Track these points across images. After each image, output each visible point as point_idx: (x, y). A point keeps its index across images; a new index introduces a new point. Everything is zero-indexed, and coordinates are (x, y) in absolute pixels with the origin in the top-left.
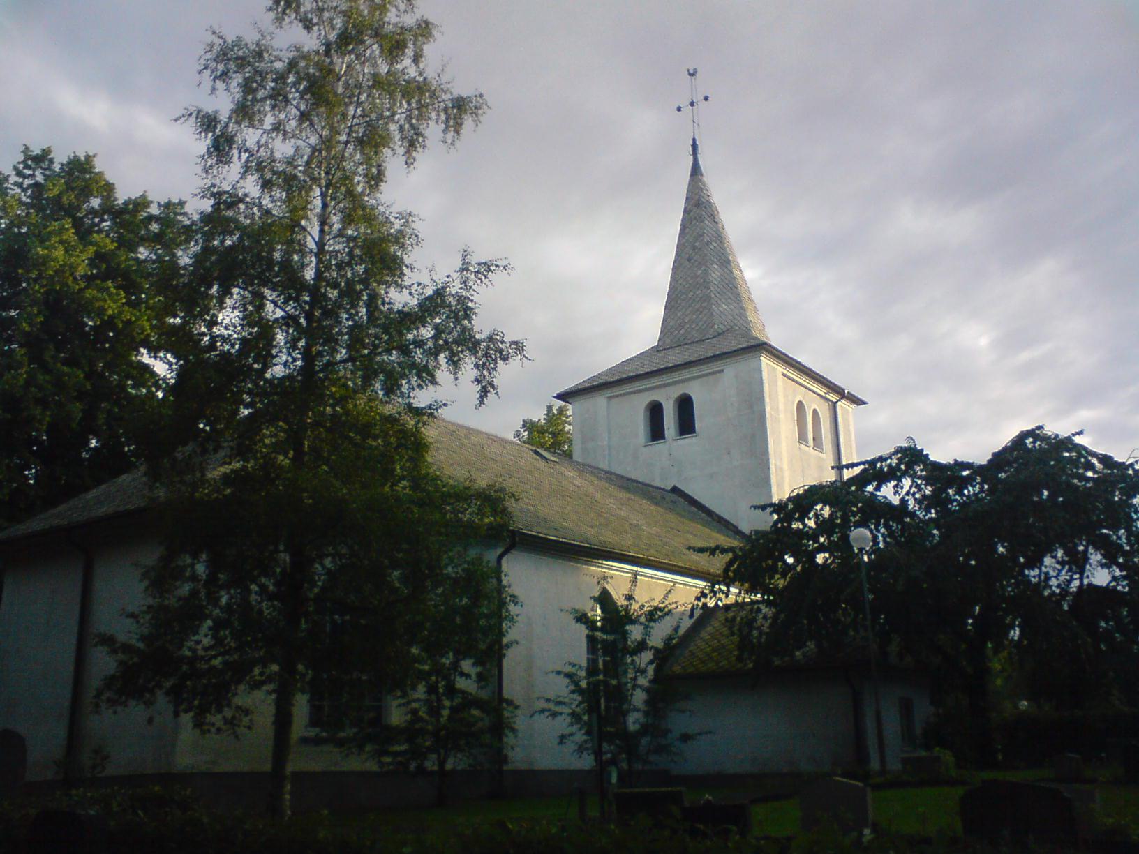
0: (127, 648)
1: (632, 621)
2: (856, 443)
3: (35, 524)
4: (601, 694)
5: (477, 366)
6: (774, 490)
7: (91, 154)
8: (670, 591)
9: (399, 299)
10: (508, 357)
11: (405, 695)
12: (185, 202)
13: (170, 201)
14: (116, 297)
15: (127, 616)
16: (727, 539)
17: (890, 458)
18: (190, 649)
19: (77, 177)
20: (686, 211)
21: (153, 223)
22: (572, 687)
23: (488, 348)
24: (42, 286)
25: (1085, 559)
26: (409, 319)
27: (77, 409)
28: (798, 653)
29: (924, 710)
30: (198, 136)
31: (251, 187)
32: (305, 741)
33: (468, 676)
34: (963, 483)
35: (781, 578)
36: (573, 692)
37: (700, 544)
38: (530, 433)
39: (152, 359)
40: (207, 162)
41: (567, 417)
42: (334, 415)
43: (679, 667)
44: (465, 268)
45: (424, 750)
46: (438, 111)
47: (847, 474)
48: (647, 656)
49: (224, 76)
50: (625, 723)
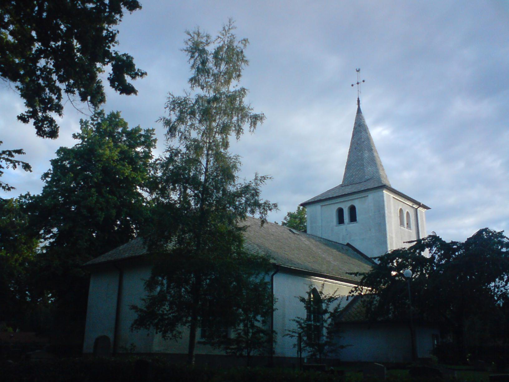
0: (141, 310)
3: (102, 259)
5: (260, 213)
6: (389, 246)
8: (336, 291)
9: (231, 189)
11: (235, 328)
12: (155, 129)
13: (149, 129)
16: (369, 266)
17: (427, 239)
20: (355, 128)
22: (299, 326)
26: (238, 195)
27: (114, 212)
32: (199, 343)
33: (259, 321)
39: (142, 190)
40: (167, 136)
44: (256, 179)
45: (242, 348)
49: (173, 109)
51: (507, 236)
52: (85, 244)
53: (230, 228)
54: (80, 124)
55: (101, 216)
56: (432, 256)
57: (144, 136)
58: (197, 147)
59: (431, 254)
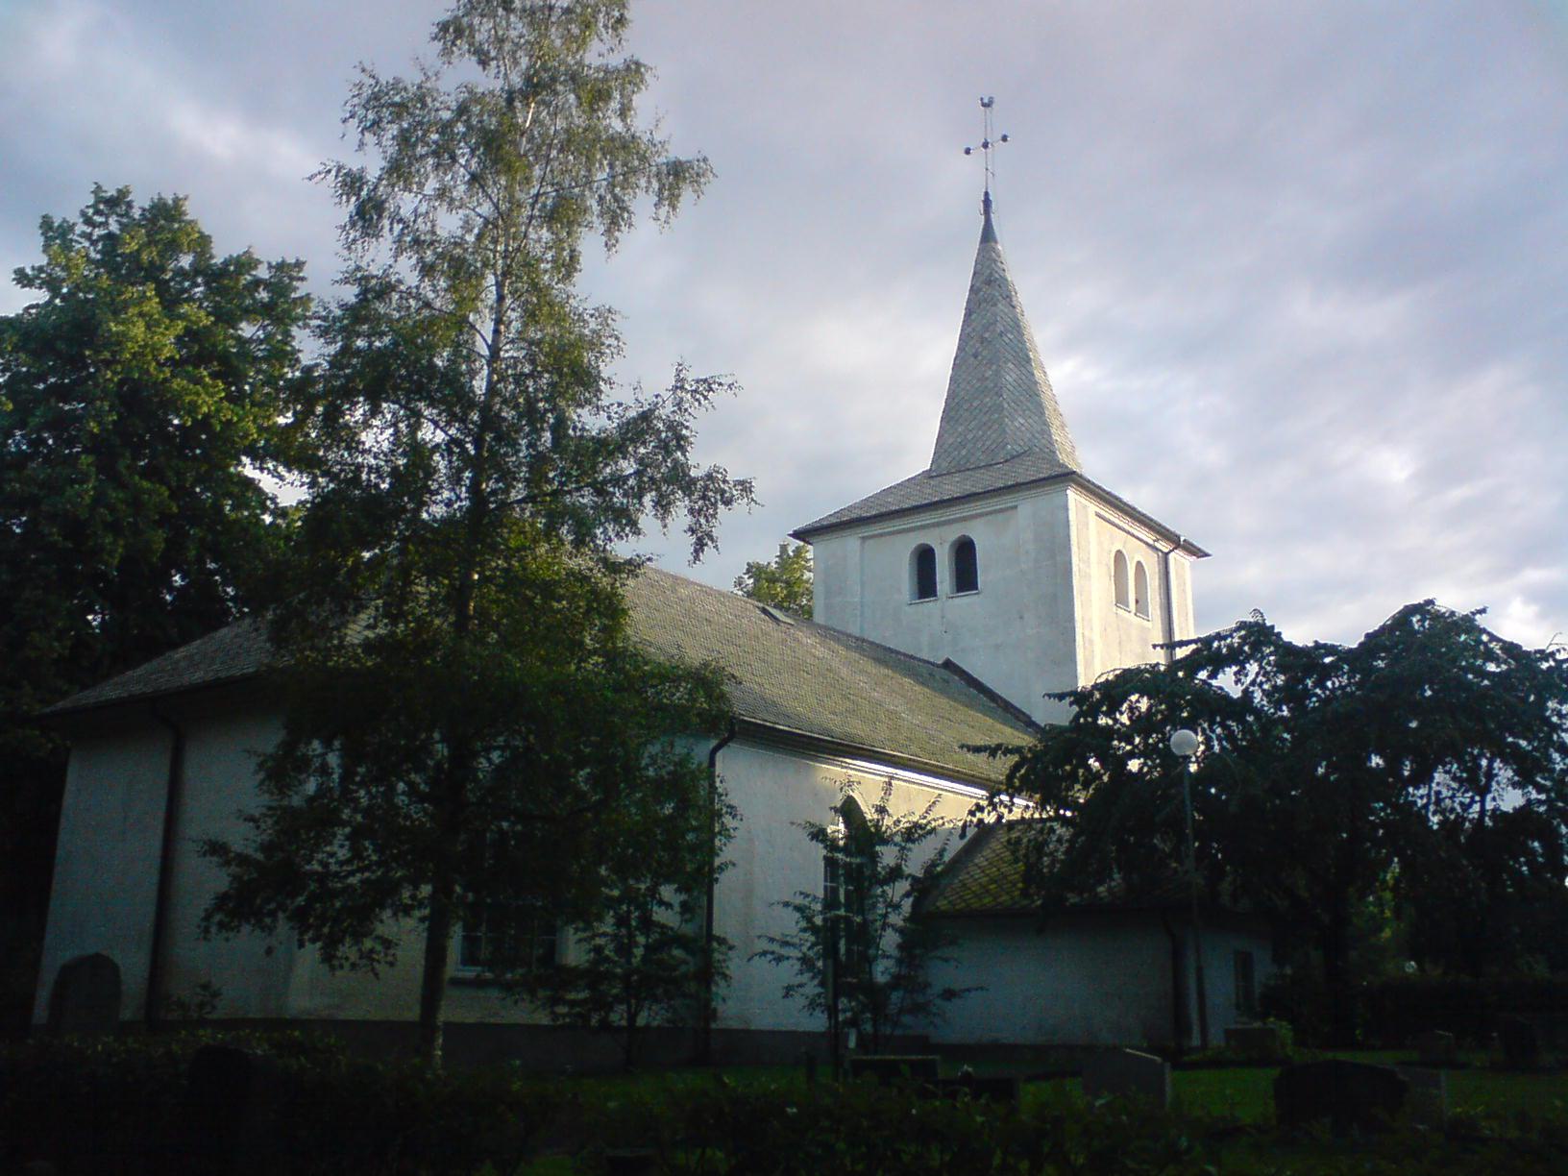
0: (243, 860)
1: (885, 841)
2: (1194, 610)
3: (110, 691)
4: (842, 934)
5: (691, 511)
6: (1080, 669)
7: (181, 196)
8: (934, 803)
9: (591, 422)
10: (731, 500)
11: (588, 926)
12: (304, 263)
13: (283, 261)
14: (211, 390)
15: (245, 820)
16: (1016, 733)
17: (1231, 636)
18: (321, 862)
19: (162, 227)
21: (261, 289)
22: (803, 924)
23: (706, 488)
24: (115, 373)
25: (1490, 775)
26: (606, 447)
27: (158, 538)
28: (1101, 889)
29: (1264, 970)
30: (337, 200)
31: (406, 271)
32: (457, 982)
33: (669, 905)
34: (1326, 672)
35: (1084, 789)
36: (804, 930)
37: (979, 740)
38: (757, 581)
39: (258, 471)
40: (348, 233)
41: (807, 561)
42: (507, 571)
43: (945, 902)
44: (679, 386)
46: (649, 177)
47: (1181, 653)
48: (903, 886)
49: (375, 126)
50: (870, 973)
51: (1489, 630)
52: (56, 644)
53: (581, 563)
54: (42, 234)
55: (113, 550)
56: (1246, 692)
57: (267, 285)
58: (458, 269)
59: (1240, 688)
